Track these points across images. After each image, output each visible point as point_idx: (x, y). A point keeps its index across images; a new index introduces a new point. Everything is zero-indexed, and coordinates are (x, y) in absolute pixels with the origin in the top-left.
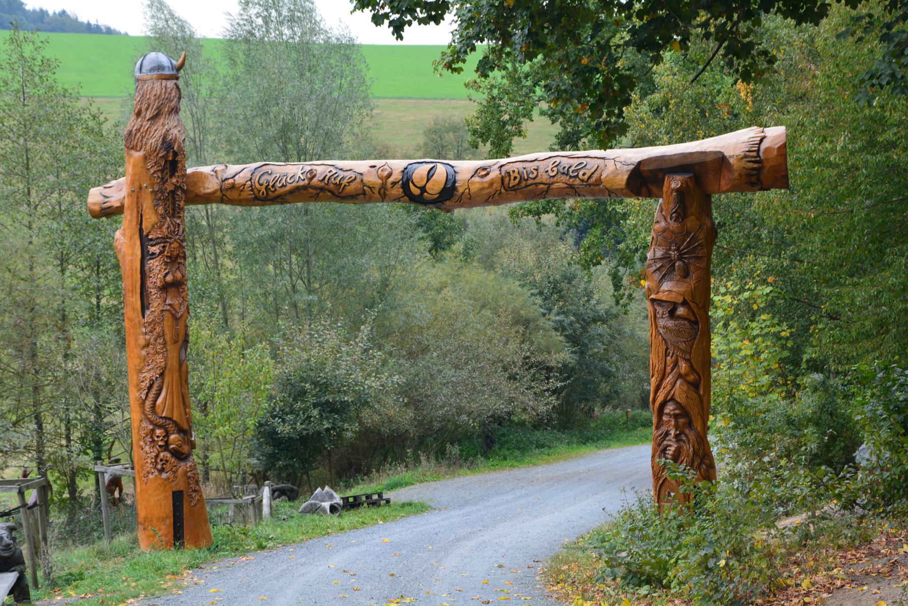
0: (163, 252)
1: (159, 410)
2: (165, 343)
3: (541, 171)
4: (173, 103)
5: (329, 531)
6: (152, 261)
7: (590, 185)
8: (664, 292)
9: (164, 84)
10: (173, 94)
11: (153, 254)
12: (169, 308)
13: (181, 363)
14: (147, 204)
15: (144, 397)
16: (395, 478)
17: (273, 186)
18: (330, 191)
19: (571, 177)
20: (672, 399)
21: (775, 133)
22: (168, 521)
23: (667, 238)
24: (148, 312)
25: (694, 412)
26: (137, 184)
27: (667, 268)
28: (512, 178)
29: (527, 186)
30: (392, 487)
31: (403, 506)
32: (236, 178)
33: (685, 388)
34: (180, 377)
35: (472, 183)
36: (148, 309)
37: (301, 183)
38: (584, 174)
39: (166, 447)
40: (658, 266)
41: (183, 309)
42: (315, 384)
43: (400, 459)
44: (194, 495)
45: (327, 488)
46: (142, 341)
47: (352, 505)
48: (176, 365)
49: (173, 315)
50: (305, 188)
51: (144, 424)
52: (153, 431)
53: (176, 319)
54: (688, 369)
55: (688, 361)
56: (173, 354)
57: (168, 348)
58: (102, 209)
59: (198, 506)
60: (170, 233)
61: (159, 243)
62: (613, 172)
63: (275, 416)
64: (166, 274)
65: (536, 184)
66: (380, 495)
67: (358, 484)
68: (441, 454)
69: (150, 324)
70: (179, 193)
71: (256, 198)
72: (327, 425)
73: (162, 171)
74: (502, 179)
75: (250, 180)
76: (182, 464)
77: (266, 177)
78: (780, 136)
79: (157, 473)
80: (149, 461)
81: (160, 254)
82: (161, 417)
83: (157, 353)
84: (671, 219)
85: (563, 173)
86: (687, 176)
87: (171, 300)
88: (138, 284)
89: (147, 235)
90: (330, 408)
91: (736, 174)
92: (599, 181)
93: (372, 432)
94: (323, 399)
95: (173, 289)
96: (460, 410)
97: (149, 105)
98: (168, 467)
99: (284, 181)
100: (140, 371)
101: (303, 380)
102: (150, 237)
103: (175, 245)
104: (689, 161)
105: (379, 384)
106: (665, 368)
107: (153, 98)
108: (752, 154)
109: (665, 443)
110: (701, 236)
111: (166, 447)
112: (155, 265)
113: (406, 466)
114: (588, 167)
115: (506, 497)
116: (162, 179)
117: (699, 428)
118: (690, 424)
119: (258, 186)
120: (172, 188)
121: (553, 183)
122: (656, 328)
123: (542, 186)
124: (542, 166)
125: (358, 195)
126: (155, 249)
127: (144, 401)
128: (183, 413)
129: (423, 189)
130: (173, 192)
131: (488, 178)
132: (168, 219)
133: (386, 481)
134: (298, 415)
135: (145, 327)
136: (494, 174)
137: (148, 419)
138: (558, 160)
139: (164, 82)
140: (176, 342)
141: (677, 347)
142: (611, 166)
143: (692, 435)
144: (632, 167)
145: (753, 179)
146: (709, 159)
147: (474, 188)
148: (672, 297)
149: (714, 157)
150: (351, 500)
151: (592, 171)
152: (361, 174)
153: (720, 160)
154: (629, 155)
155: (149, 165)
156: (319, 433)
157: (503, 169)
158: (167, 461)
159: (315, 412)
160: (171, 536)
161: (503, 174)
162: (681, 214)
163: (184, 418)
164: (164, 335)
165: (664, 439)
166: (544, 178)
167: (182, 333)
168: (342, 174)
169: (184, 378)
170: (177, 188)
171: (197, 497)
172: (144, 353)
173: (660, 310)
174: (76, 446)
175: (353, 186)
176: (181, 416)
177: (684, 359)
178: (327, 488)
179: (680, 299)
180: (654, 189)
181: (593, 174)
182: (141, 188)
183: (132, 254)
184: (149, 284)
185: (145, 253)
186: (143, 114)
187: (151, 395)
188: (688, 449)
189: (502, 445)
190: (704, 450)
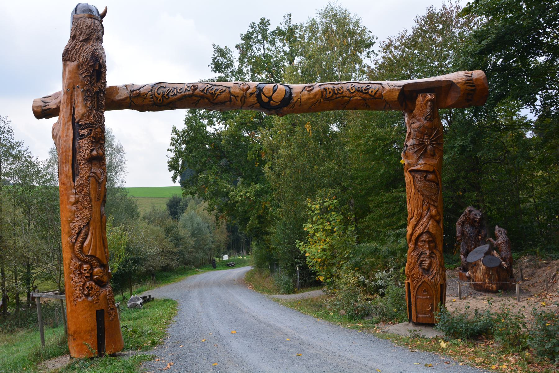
1: (85, 250)
2: (90, 201)
6: (81, 141)
7: (375, 98)
11: (83, 135)
13: (101, 215)
14: (79, 99)
15: (74, 241)
17: (167, 95)
18: (207, 99)
19: (364, 93)
24: (77, 178)
28: (328, 92)
29: (337, 98)
32: (141, 90)
33: (435, 224)
36: (78, 176)
37: (187, 93)
38: (372, 92)
39: (91, 278)
46: (72, 199)
48: (98, 216)
49: (96, 180)
50: (190, 96)
51: (74, 261)
52: (81, 266)
56: (96, 209)
57: (93, 203)
58: (43, 110)
59: (115, 320)
61: (87, 128)
64: (92, 150)
65: (343, 97)
69: (79, 186)
70: (102, 95)
73: (91, 76)
75: (151, 91)
76: (103, 290)
77: (162, 89)
79: (84, 298)
80: (78, 288)
83: (85, 208)
84: (425, 120)
88: (70, 158)
92: (381, 95)
98: (92, 292)
100: (71, 222)
102: (80, 123)
111: (91, 278)
112: (84, 143)
119: (157, 95)
121: (353, 97)
123: (346, 98)
126: (85, 132)
127: (74, 244)
128: (103, 252)
129: (270, 98)
135: (75, 189)
140: (98, 200)
148: (427, 168)
152: (229, 87)
153: (450, 84)
158: (92, 288)
164: (90, 194)
166: (347, 93)
167: (103, 194)
168: (215, 88)
171: (114, 313)
172: (74, 208)
174: (19, 282)
175: (223, 95)
177: (434, 206)
181: (377, 91)
182: (74, 88)
184: (78, 157)
185: (77, 135)
186: (77, 37)
187: (80, 239)
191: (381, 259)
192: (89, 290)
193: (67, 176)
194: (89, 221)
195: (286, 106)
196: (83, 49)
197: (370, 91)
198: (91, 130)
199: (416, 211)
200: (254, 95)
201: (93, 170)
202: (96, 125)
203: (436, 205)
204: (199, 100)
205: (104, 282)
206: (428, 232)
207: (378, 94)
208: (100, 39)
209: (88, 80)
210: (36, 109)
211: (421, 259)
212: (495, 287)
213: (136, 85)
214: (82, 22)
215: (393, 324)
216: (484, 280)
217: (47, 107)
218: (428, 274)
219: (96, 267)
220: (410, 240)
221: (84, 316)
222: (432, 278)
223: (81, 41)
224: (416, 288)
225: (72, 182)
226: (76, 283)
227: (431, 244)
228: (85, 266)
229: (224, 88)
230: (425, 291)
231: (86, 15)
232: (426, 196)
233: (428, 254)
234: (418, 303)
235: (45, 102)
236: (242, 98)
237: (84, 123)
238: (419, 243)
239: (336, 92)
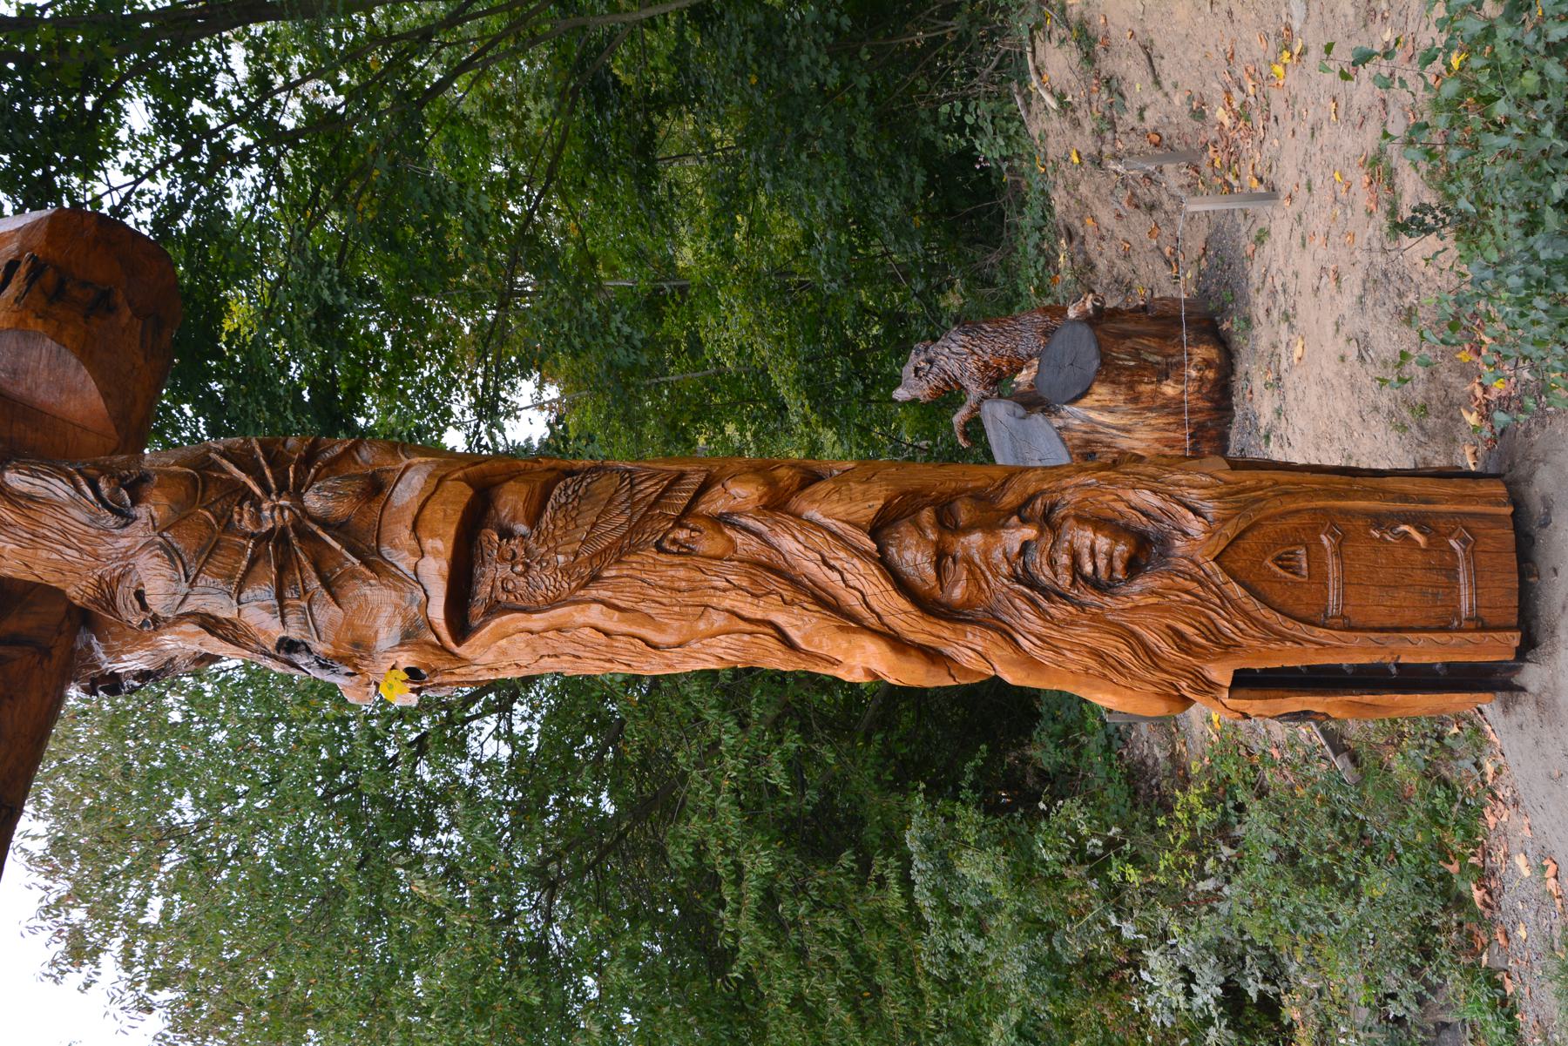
33: (822, 488)
177: (704, 488)
191: (1071, 1004)
203: (696, 479)
206: (879, 528)
211: (1065, 580)
212: (1202, 352)
215: (1484, 876)
216: (1173, 408)
218: (1165, 542)
220: (932, 656)
222: (1196, 512)
224: (1274, 619)
230: (1285, 562)
232: (635, 529)
233: (1029, 533)
234: (1380, 616)
238: (958, 593)
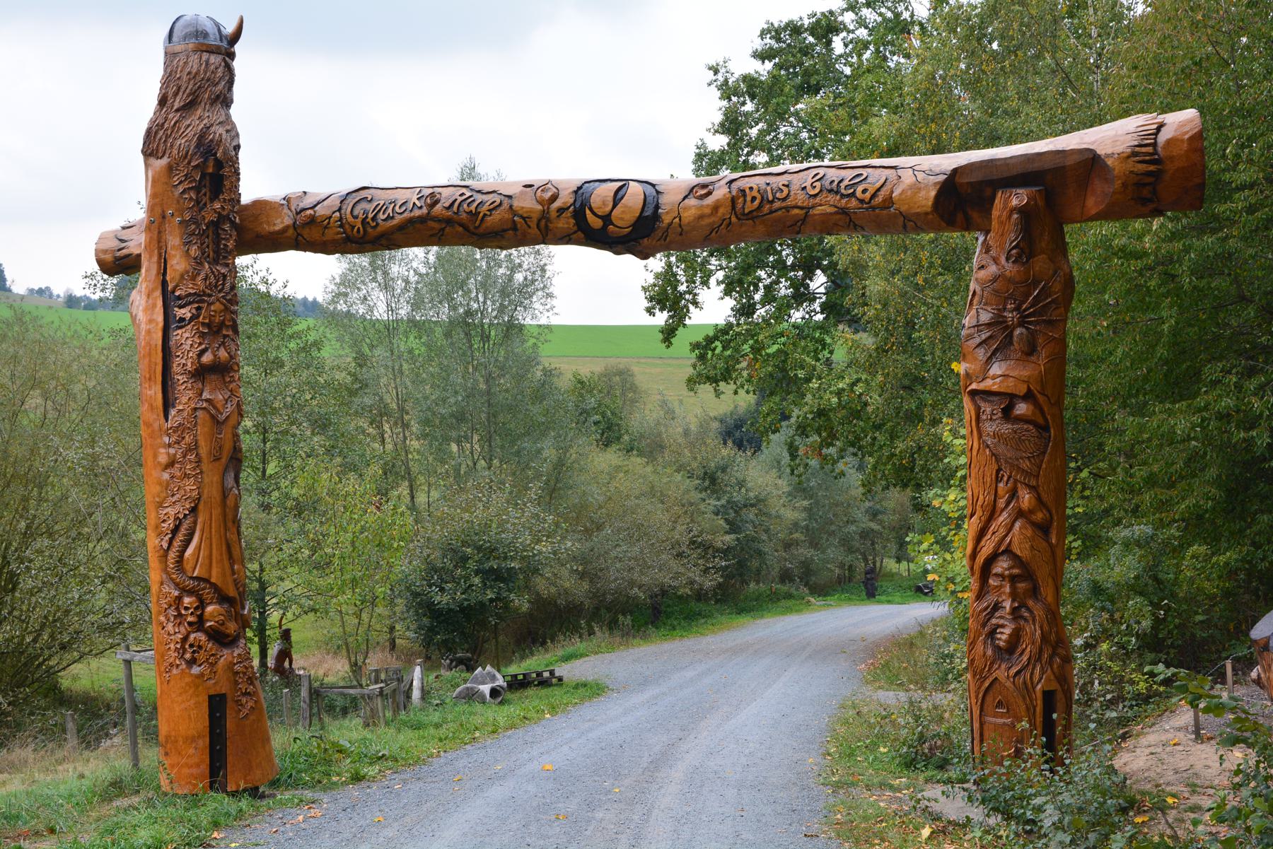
0: (198, 316)
1: (188, 567)
3: (794, 187)
4: (220, 87)
5: (477, 734)
6: (180, 331)
7: (874, 208)
8: (994, 378)
9: (204, 58)
10: (219, 74)
11: (182, 320)
12: (205, 405)
13: (225, 494)
14: (174, 240)
15: (165, 545)
16: (570, 649)
17: (374, 218)
18: (461, 225)
19: (843, 196)
20: (1008, 551)
21: (1181, 121)
22: (201, 743)
23: (1001, 291)
24: (173, 412)
25: (1042, 573)
26: (158, 210)
27: (999, 339)
28: (749, 199)
29: (771, 212)
30: (567, 658)
31: (577, 687)
33: (1029, 533)
34: (224, 515)
35: (687, 208)
37: (417, 213)
38: (864, 191)
39: (199, 625)
40: (984, 337)
41: (230, 408)
42: (479, 549)
43: (575, 630)
44: (244, 700)
45: (488, 668)
46: (163, 459)
47: (518, 684)
49: (213, 417)
50: (422, 220)
51: (166, 589)
52: (179, 598)
53: (217, 423)
54: (1033, 501)
55: (1033, 489)
56: (211, 477)
57: (205, 467)
58: (117, 259)
59: (252, 717)
60: (210, 286)
61: (190, 303)
62: (911, 187)
63: (434, 584)
65: (788, 209)
66: (552, 672)
67: (532, 654)
68: (612, 625)
69: (176, 429)
70: (227, 227)
71: (348, 239)
72: (490, 595)
73: (197, 189)
74: (733, 200)
75: (340, 210)
76: (225, 651)
77: (364, 205)
78: (1191, 120)
79: (184, 666)
80: (172, 646)
81: (191, 319)
82: (192, 578)
83: (186, 476)
84: (1007, 259)
85: (830, 191)
86: (1034, 189)
87: (211, 392)
88: (159, 369)
89: (173, 292)
90: (496, 576)
91: (1118, 184)
92: (889, 201)
93: (550, 603)
94: (487, 566)
95: (213, 377)
96: (632, 583)
97: (179, 88)
98: (201, 656)
99: (390, 211)
100: (160, 505)
101: (465, 544)
102: (177, 294)
103: (217, 306)
104: (1036, 166)
105: (554, 557)
106: (995, 501)
107: (185, 78)
108: (1144, 150)
109: (994, 621)
110: (1057, 287)
111: (199, 625)
112: (185, 338)
113: (580, 637)
114: (869, 180)
115: (689, 674)
116: (198, 202)
117: (1050, 599)
118: (1034, 592)
119: (350, 219)
120: (214, 217)
121: (813, 207)
122: (980, 437)
123: (796, 211)
124: (797, 181)
125: (504, 231)
126: (185, 313)
128: (228, 572)
129: (607, 219)
130: (216, 225)
131: (710, 200)
132: (207, 266)
133: (560, 653)
134: (458, 583)
135: (169, 435)
136: (720, 192)
137: (172, 580)
138: (822, 172)
139: (205, 56)
140: (217, 459)
141: (1015, 467)
142: (908, 178)
143: (1039, 610)
144: (942, 178)
145: (1146, 192)
146: (1070, 161)
147: (688, 216)
148: (1009, 386)
149: (1077, 158)
150: (521, 677)
151: (878, 185)
152: (510, 197)
153: (1090, 162)
154: (936, 162)
155: (176, 180)
156: (482, 604)
157: (735, 186)
158: (200, 647)
159: (477, 580)
160: (205, 768)
161: (734, 193)
162: (1024, 251)
163: (230, 580)
165: (991, 615)
166: (800, 198)
167: (228, 446)
168: (479, 198)
169: (230, 517)
170: (222, 218)
171: (251, 704)
172: (166, 476)
173: (987, 408)
175: (497, 216)
176: (224, 575)
177: (1027, 485)
178: (488, 668)
179: (1022, 390)
180: (975, 215)
181: (879, 190)
182: (164, 217)
183: (150, 321)
184: (176, 368)
188: (1033, 631)
189: (668, 617)
190: (1057, 633)
192: (194, 652)
193: (152, 407)
194: (196, 506)
195: (648, 236)
196: (179, 128)
197: (860, 189)
198: (198, 309)
199: (981, 497)
200: (568, 214)
201: (206, 395)
202: (210, 296)
204: (443, 229)
205: (228, 636)
207: (879, 199)
208: (225, 100)
209: (191, 199)
210: (103, 257)
211: (994, 621)
213: (314, 194)
214: (181, 63)
217: (124, 252)
219: (210, 603)
221: (183, 706)
223: (177, 110)
225: (163, 420)
226: (169, 634)
227: (1020, 585)
228: (187, 600)
229: (498, 199)
231: (191, 46)
235: (122, 241)
236: (539, 221)
237: (183, 293)
238: (991, 581)
239: (771, 198)
